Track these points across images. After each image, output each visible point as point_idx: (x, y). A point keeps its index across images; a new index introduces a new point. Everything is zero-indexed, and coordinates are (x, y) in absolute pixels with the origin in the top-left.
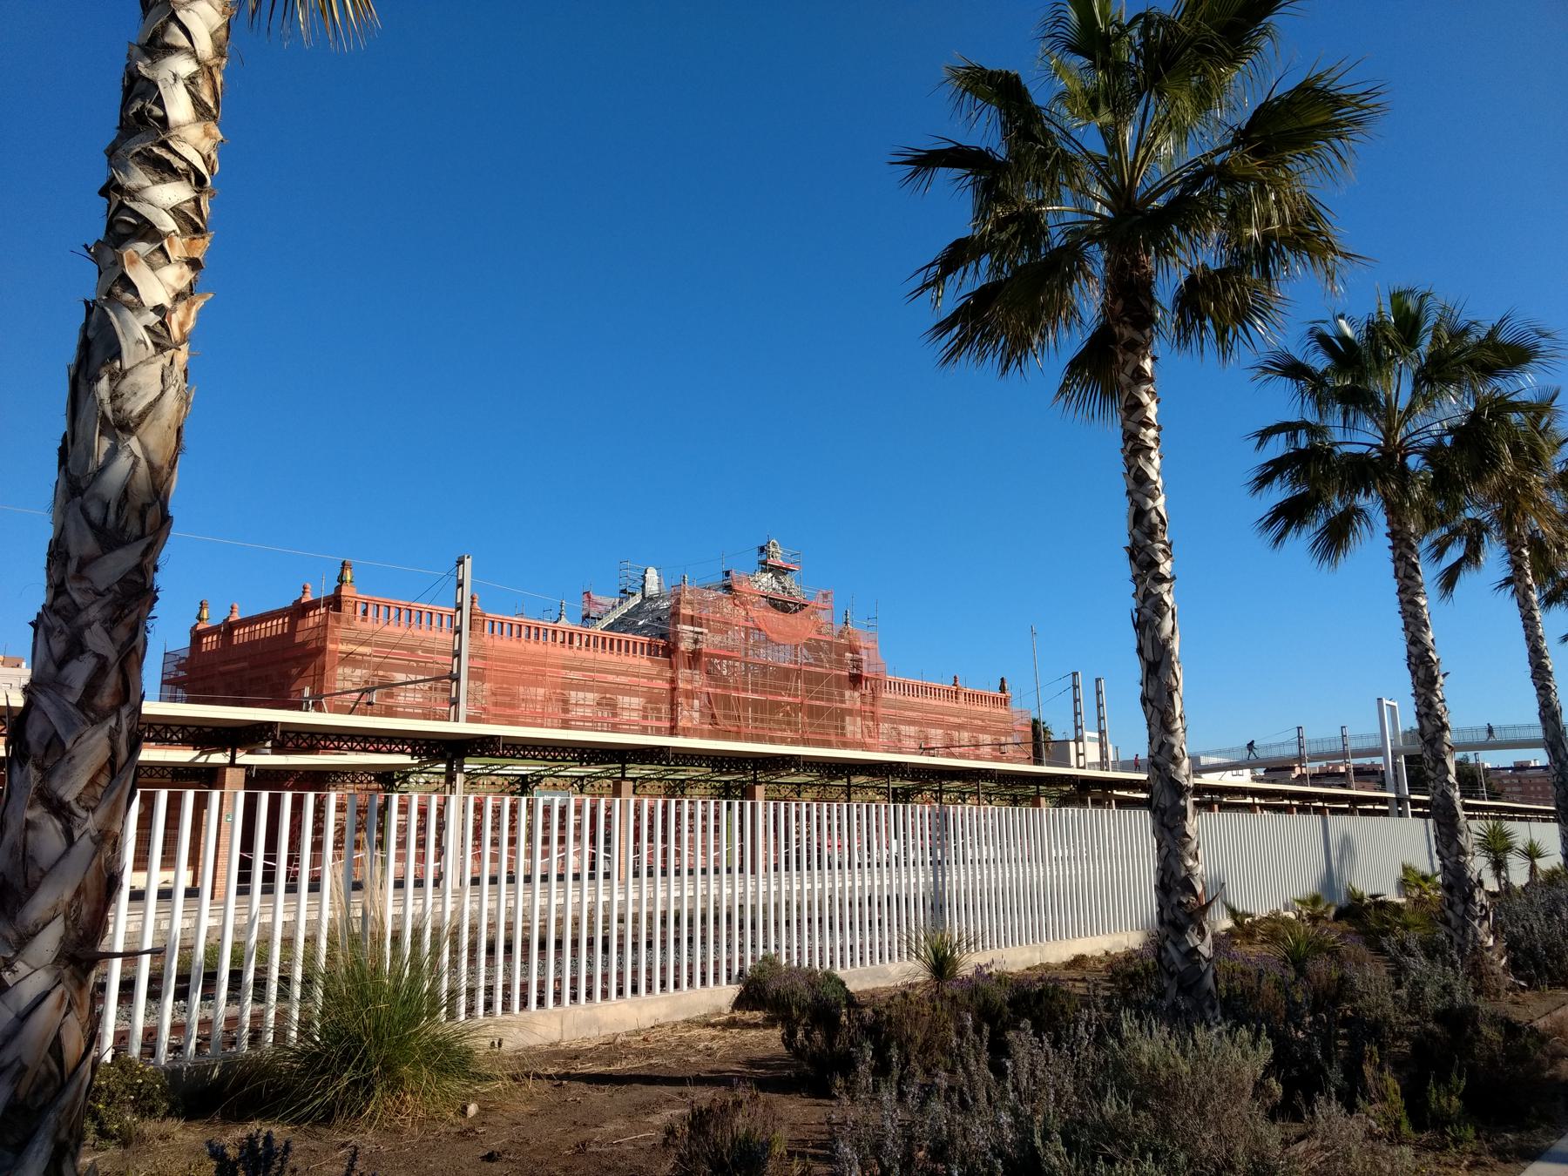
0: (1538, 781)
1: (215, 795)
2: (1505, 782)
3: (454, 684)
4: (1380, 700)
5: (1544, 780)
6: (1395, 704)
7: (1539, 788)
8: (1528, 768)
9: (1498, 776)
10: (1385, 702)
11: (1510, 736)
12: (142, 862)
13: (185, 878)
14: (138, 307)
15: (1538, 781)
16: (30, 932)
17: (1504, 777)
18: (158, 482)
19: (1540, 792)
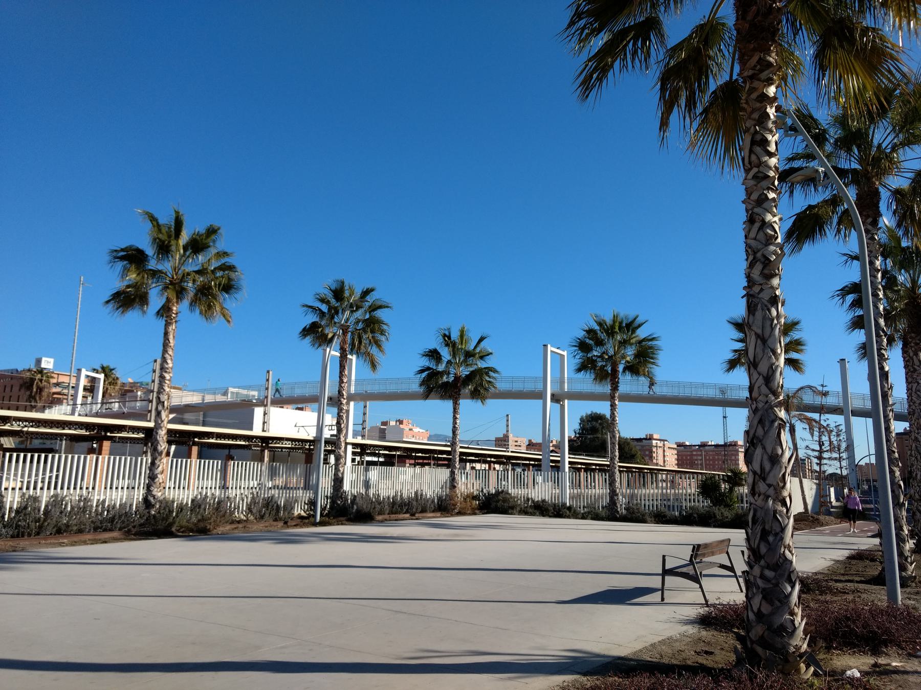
0: (711, 453)
1: (100, 457)
2: (694, 453)
3: (150, 404)
4: (545, 346)
5: (714, 453)
6: (565, 353)
7: (688, 458)
8: (707, 446)
9: (690, 450)
10: (550, 348)
11: (518, 387)
12: (8, 479)
13: (19, 485)
14: (770, 168)
15: (711, 453)
16: (152, 488)
17: (694, 451)
18: (757, 360)
19: (711, 460)
